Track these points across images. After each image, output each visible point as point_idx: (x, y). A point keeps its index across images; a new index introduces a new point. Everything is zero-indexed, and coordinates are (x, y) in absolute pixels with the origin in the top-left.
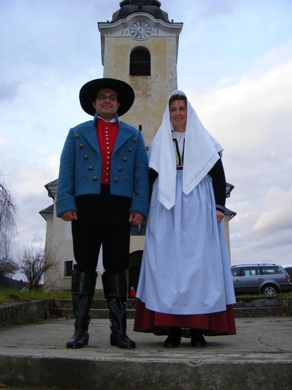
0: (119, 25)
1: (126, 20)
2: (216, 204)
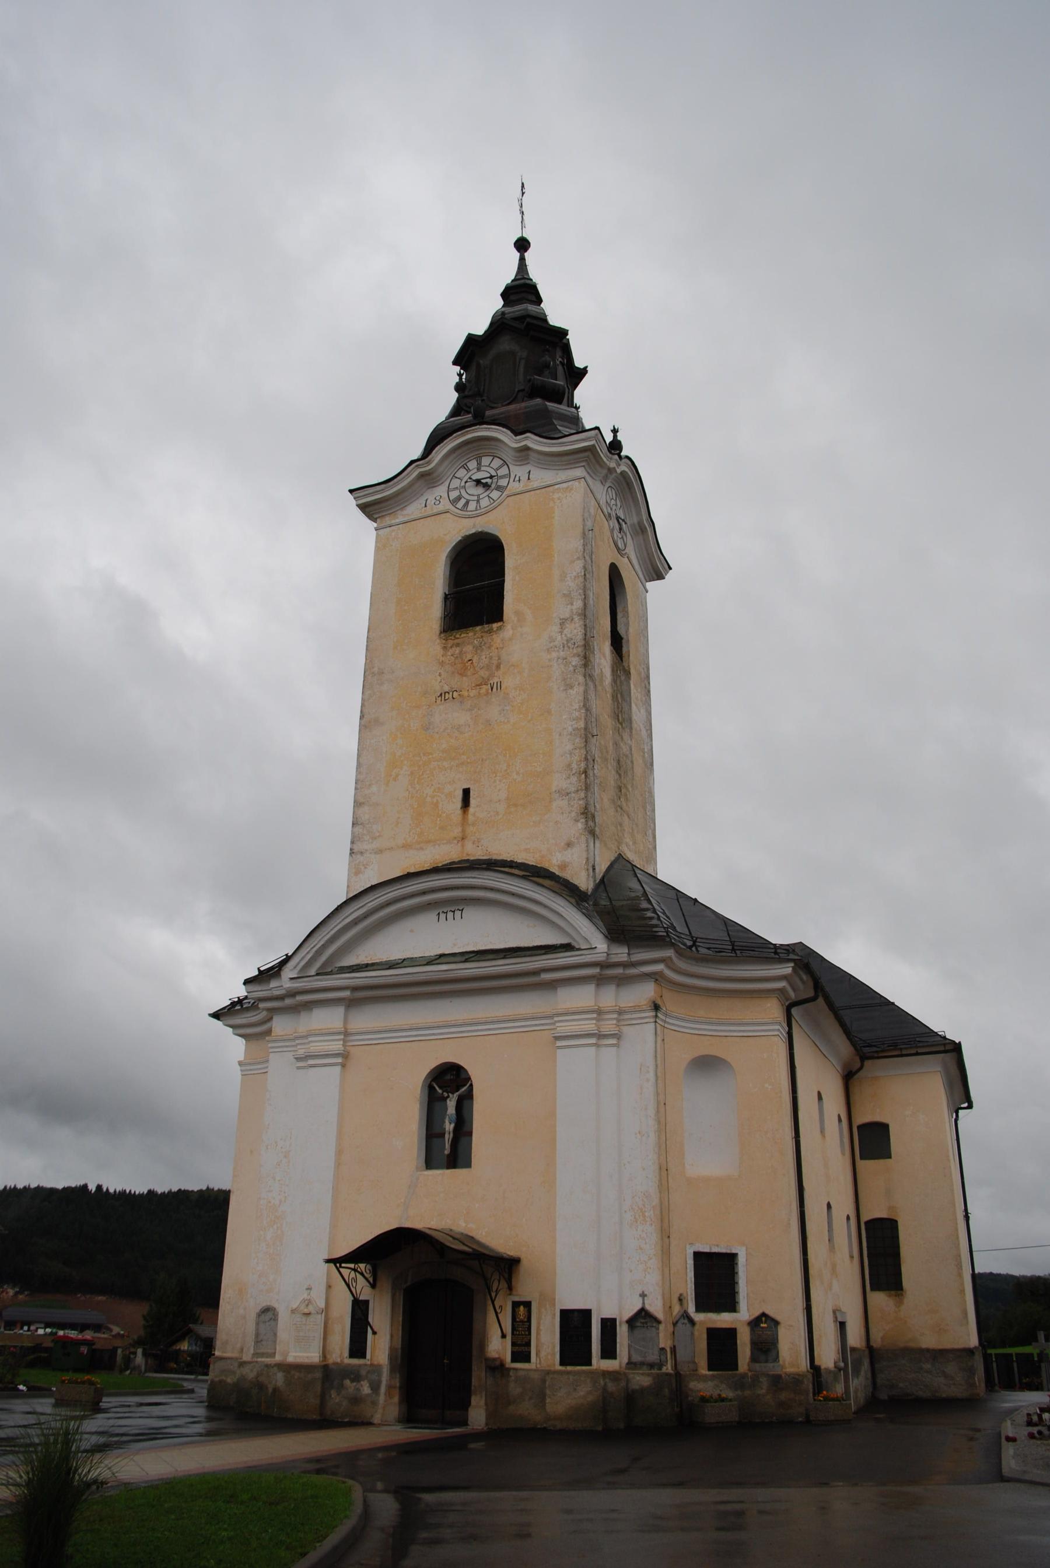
0: (411, 485)
1: (429, 463)
2: (560, 403)
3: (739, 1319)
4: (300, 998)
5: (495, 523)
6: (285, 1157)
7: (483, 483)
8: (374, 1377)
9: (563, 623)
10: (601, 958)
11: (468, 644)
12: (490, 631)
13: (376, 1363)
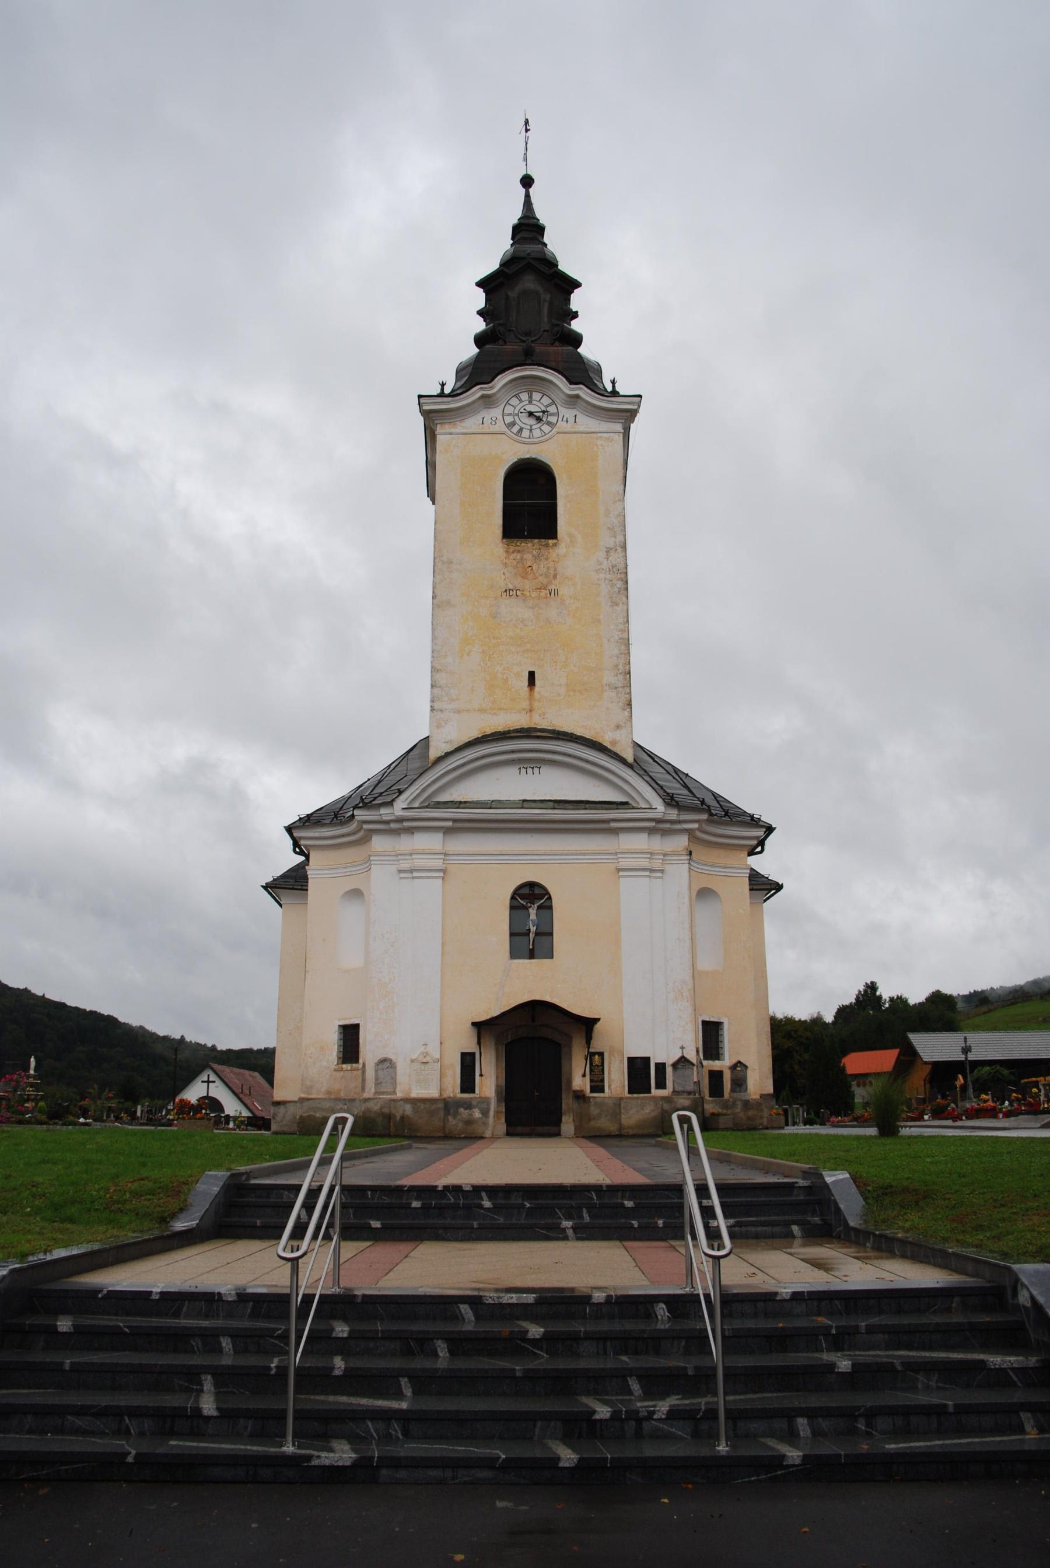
0: (473, 402)
1: (492, 388)
3: (723, 1064)
4: (406, 824)
5: (549, 453)
6: (392, 946)
7: (535, 416)
8: (485, 1106)
9: (608, 551)
10: (659, 816)
11: (528, 553)
12: (547, 545)
13: (483, 1096)
